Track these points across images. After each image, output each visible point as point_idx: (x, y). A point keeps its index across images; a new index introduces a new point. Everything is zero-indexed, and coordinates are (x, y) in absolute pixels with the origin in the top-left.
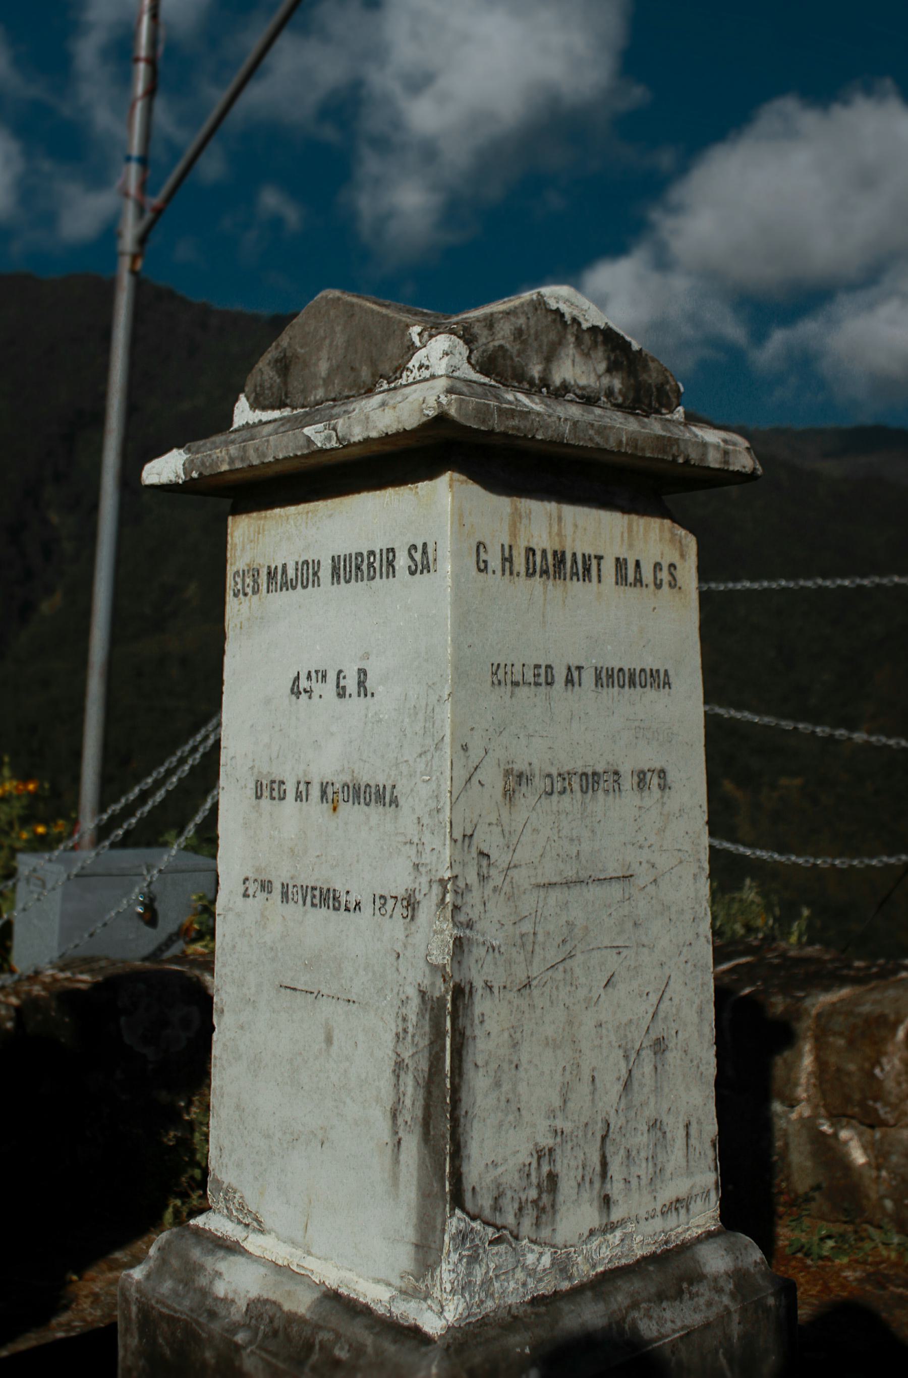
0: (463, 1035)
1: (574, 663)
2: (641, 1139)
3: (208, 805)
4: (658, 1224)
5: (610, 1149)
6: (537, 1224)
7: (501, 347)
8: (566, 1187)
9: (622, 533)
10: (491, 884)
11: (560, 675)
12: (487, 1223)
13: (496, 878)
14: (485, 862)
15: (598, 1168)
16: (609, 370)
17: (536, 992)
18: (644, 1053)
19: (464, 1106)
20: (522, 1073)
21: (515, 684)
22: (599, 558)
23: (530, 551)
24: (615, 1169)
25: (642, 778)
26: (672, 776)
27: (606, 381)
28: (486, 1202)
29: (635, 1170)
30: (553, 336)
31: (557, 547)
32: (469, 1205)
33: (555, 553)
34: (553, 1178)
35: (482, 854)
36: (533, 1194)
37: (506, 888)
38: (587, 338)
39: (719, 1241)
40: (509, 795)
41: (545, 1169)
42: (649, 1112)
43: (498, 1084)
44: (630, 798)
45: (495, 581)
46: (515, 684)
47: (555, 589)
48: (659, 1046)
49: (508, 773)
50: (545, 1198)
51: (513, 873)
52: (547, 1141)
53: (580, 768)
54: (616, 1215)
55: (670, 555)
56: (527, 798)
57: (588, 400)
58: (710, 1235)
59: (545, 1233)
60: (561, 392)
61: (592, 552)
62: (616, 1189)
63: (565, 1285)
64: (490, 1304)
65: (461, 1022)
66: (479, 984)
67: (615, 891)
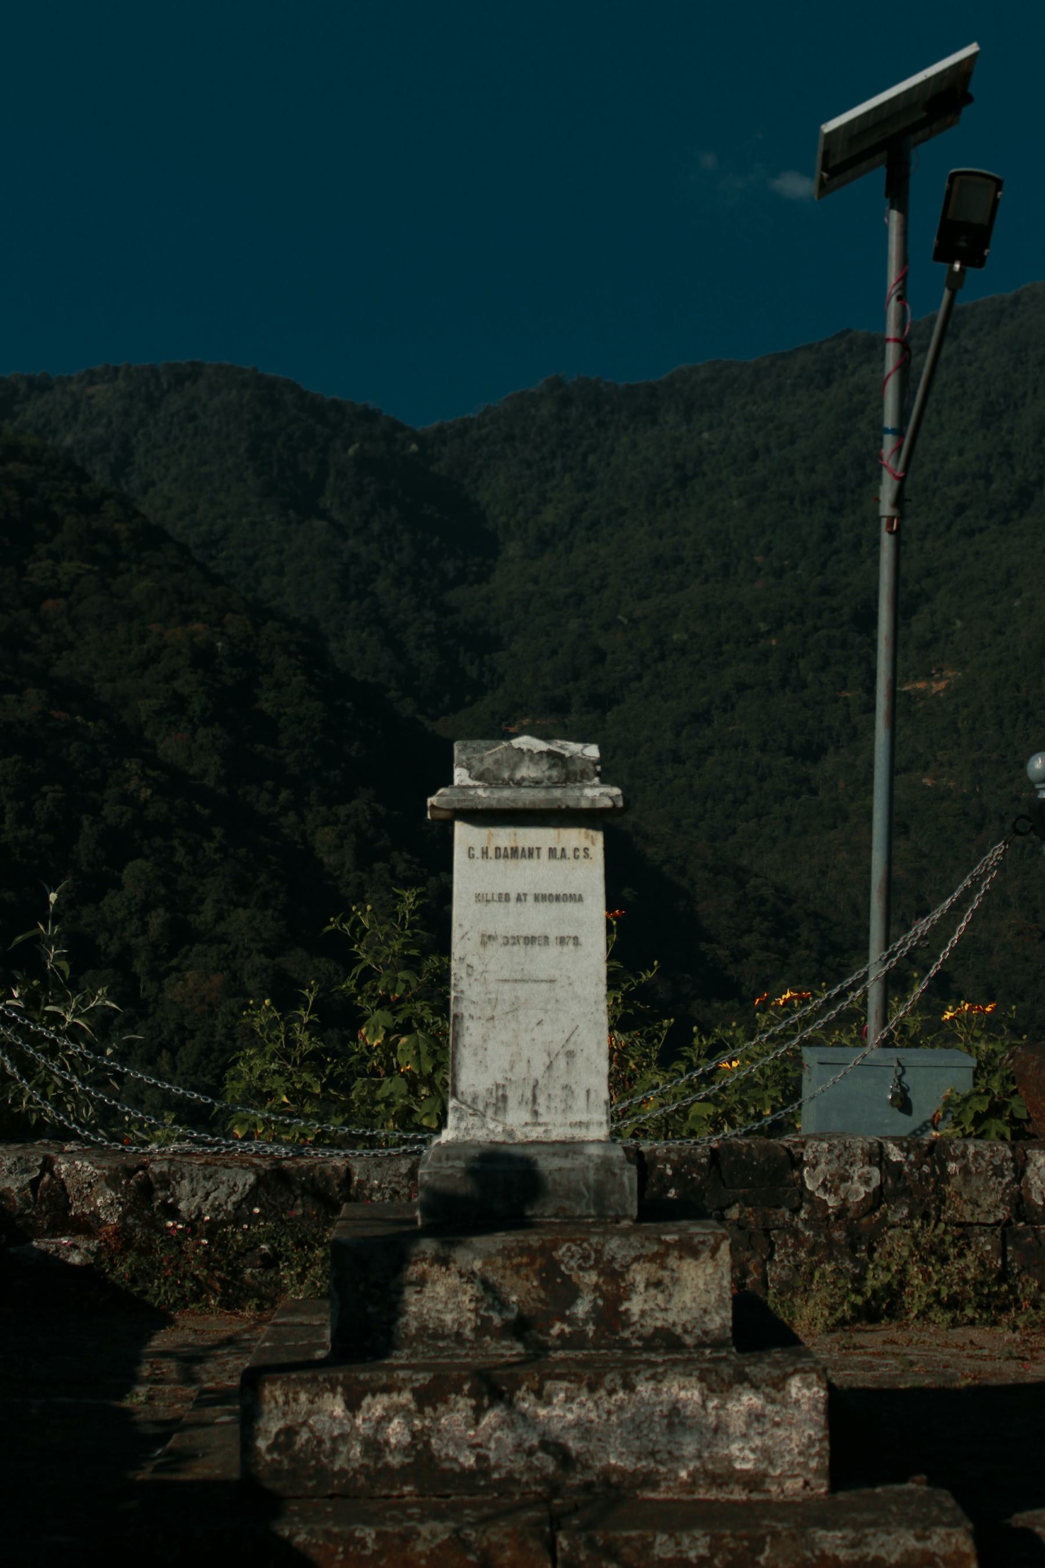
0: (458, 1033)
1: (521, 891)
2: (558, 1091)
3: (863, 971)
4: (948, 1357)
5: (538, 1092)
6: (496, 1113)
7: (488, 769)
8: (512, 1102)
9: (500, 854)
10: (473, 978)
11: (513, 896)
12: (469, 1107)
13: (476, 975)
14: (470, 970)
15: (531, 1098)
16: (550, 768)
17: (496, 1022)
18: (560, 1057)
19: (457, 1061)
20: (488, 1052)
21: (488, 901)
22: (538, 849)
23: (497, 849)
24: (542, 1100)
25: (562, 941)
26: (582, 940)
27: (547, 773)
28: (469, 1100)
29: (553, 1105)
30: (516, 759)
31: (513, 845)
32: (460, 1097)
33: (512, 849)
34: (504, 1098)
35: (468, 966)
36: (493, 1101)
37: (482, 980)
38: (537, 757)
39: (604, 1145)
40: (483, 944)
41: (500, 1092)
42: (563, 1081)
43: (476, 1054)
44: (554, 950)
45: (479, 862)
46: (488, 901)
47: (511, 863)
48: (570, 1054)
49: (483, 936)
50: (500, 1104)
51: (485, 975)
52: (501, 1082)
53: (524, 934)
54: (541, 1120)
55: (587, 843)
56: (493, 947)
57: (536, 783)
58: (599, 1141)
59: (500, 1118)
60: (519, 784)
61: (535, 846)
62: (542, 1110)
63: (511, 1142)
64: (468, 1138)
65: (457, 1028)
66: (466, 1015)
67: (544, 986)
